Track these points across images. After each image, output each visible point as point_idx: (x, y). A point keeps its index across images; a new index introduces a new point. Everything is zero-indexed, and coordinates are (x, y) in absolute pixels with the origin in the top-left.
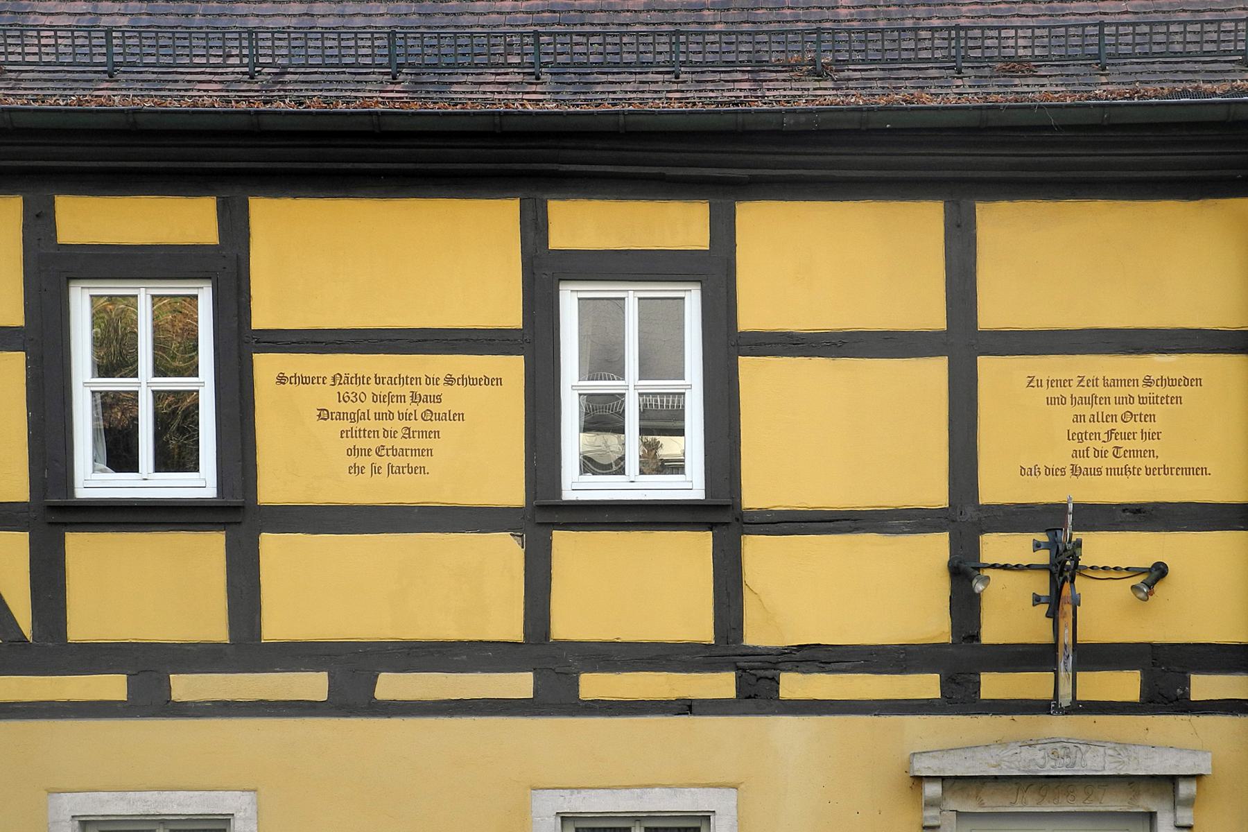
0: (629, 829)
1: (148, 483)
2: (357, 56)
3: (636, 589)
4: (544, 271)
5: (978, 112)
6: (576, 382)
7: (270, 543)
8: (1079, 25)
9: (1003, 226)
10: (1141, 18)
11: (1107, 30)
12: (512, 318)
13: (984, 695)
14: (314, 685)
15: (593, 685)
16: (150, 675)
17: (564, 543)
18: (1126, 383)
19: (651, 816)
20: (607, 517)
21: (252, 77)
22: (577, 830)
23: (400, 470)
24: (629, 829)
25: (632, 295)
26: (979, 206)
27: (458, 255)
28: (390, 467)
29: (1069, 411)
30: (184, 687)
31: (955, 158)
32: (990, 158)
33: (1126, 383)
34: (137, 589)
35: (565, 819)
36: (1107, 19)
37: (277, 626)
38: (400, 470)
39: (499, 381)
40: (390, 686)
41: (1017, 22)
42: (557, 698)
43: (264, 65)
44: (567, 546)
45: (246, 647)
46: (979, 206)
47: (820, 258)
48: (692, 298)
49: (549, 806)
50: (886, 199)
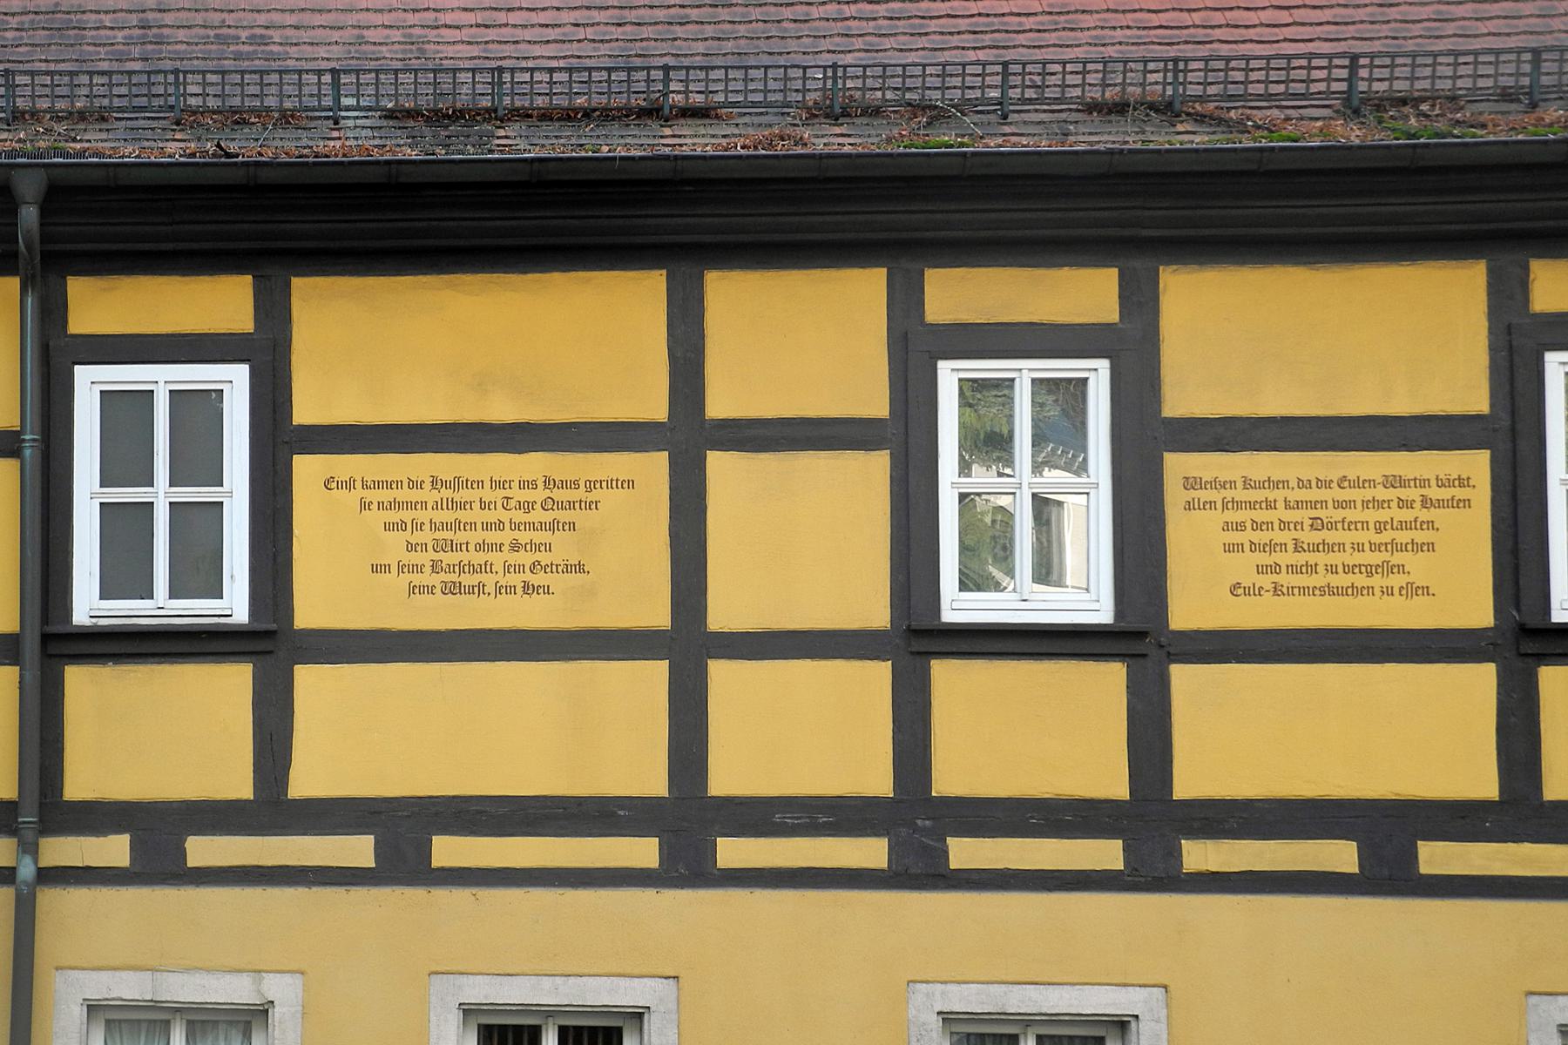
0: (1101, 1040)
1: (161, 606)
2: (746, 92)
3: (801, 732)
4: (914, 349)
5: (386, 168)
6: (956, 479)
7: (1183, 677)
8: (199, 72)
9: (729, 295)
10: (211, 65)
11: (344, 79)
12: (1477, 400)
13: (436, 862)
14: (359, 850)
15: (964, 852)
16: (159, 840)
17: (946, 675)
18: (389, 485)
19: (1054, 1019)
20: (184, 647)
21: (336, 123)
22: (1039, 1038)
23: (1291, 591)
24: (1101, 1040)
25: (1025, 372)
26: (297, 283)
27: (587, 334)
28: (526, 586)
29: (1218, 517)
30: (202, 850)
31: (381, 225)
32: (363, 225)
33: (389, 485)
34: (155, 735)
35: (947, 1018)
36: (186, 65)
37: (308, 779)
38: (1291, 591)
39: (631, 484)
40: (448, 850)
41: (766, 60)
42: (919, 869)
43: (348, 109)
44: (950, 678)
45: (272, 808)
46: (297, 283)
47: (801, 334)
48: (1098, 375)
49: (927, 1005)
50: (586, 268)
